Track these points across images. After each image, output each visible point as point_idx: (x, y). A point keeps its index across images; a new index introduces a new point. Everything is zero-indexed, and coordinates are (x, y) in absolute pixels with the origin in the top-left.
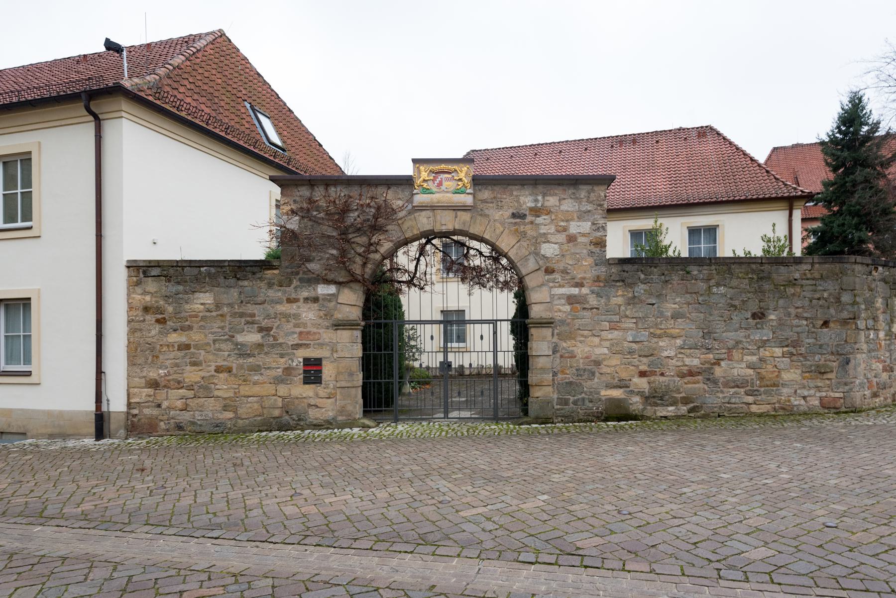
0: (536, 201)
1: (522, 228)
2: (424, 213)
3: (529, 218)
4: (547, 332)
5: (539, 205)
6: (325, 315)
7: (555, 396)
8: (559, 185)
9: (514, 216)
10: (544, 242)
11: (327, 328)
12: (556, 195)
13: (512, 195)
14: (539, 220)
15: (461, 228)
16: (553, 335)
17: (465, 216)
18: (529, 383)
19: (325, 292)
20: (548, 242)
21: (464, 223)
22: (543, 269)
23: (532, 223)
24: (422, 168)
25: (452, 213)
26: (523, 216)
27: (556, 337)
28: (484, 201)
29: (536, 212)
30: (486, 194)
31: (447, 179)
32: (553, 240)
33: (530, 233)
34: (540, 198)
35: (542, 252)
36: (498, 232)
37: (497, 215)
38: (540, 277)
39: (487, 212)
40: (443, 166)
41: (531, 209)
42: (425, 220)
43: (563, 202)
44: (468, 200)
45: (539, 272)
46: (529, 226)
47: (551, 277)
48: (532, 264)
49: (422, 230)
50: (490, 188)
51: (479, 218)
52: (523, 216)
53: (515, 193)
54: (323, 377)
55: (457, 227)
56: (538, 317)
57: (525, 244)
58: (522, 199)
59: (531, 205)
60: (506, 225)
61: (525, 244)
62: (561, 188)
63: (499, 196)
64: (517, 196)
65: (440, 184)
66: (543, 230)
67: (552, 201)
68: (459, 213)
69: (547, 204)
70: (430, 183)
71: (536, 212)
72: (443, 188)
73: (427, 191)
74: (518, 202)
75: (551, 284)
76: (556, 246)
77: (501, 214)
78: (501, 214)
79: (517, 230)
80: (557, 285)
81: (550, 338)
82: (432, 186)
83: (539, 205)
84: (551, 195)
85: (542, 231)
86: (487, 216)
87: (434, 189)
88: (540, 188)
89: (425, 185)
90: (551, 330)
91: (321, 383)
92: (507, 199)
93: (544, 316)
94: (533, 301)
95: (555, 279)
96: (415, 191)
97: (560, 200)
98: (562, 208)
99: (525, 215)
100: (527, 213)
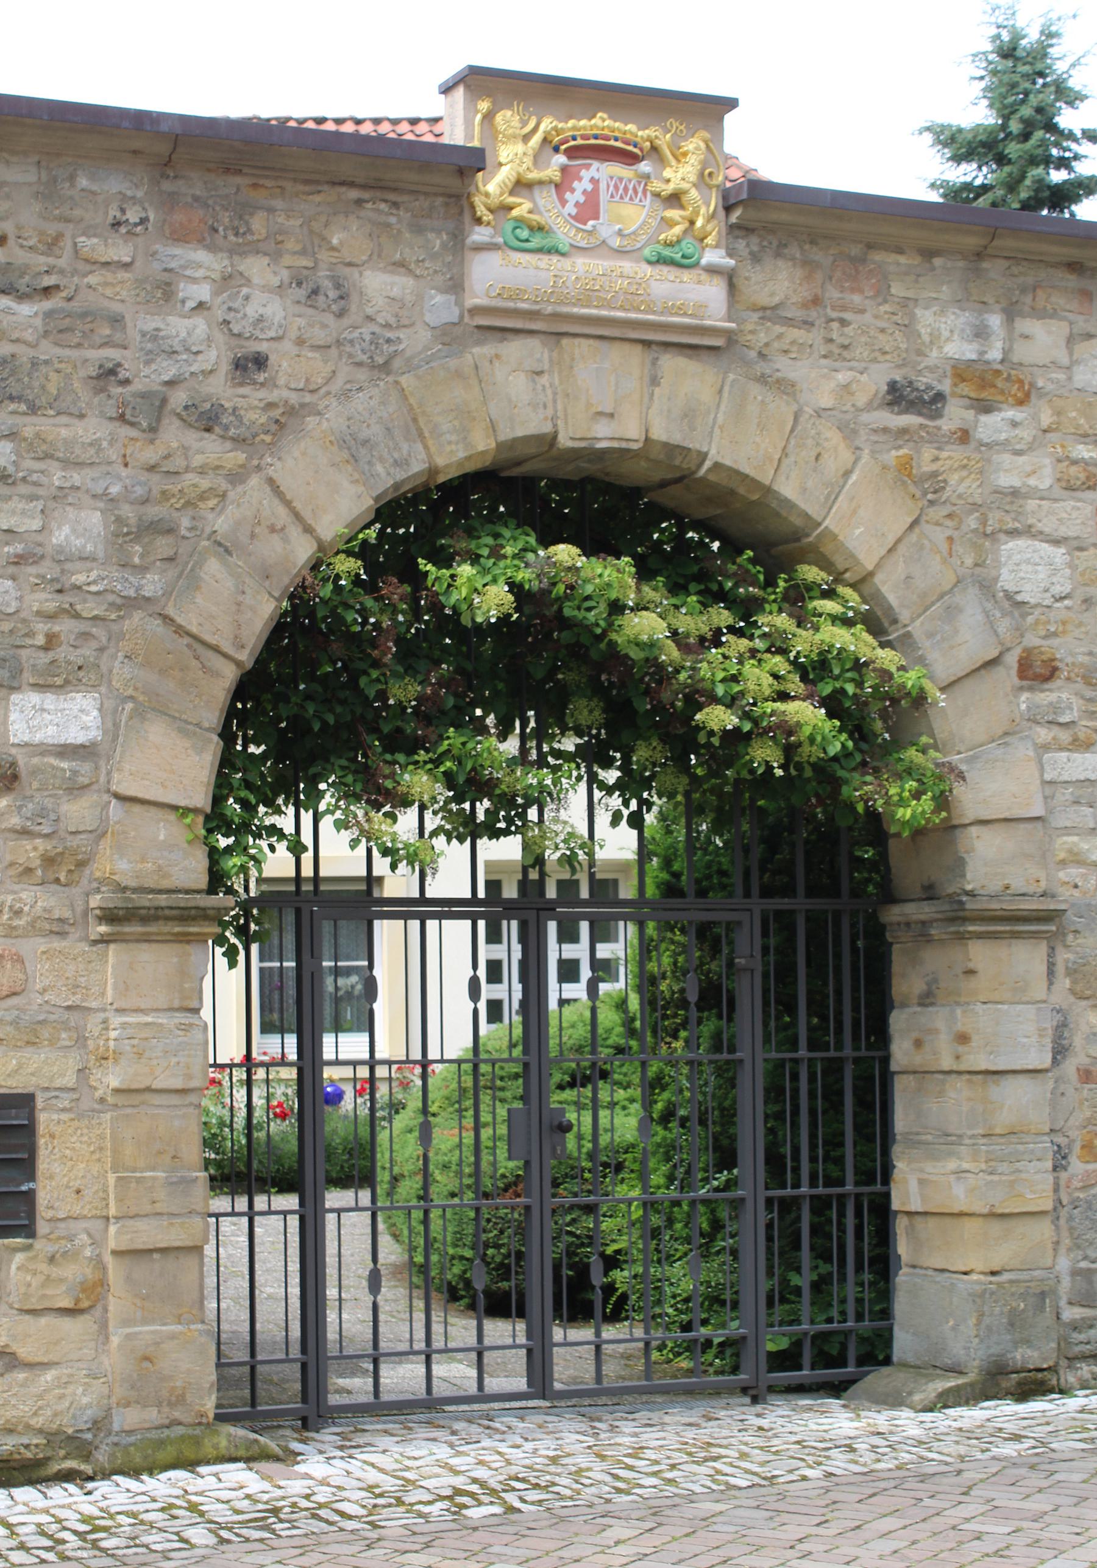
0: (981, 333)
1: (926, 459)
2: (514, 349)
3: (955, 415)
4: (1026, 959)
5: (995, 354)
6: (49, 861)
7: (1064, 1264)
8: (377, 186)
9: (898, 396)
10: (1013, 533)
11: (59, 929)
12: (1054, 315)
13: (882, 294)
14: (990, 426)
15: (676, 438)
16: (1051, 972)
17: (689, 380)
18: (895, 1205)
19: (50, 733)
20: (1028, 532)
21: (689, 415)
22: (1012, 659)
23: (964, 436)
24: (507, 119)
25: (629, 362)
26: (930, 404)
27: (1064, 983)
28: (770, 313)
29: (986, 385)
30: (778, 282)
31: (621, 191)
32: (1047, 525)
33: (962, 485)
34: (995, 321)
35: (1007, 580)
36: (832, 466)
37: (821, 383)
38: (1002, 698)
39: (784, 367)
40: (602, 122)
41: (962, 372)
42: (518, 386)
43: (1082, 349)
44: (703, 299)
45: (999, 672)
46: (953, 454)
47: (1045, 697)
48: (969, 637)
49: (506, 434)
50: (794, 250)
51: (756, 390)
52: (930, 404)
53: (897, 289)
54: (42, 1199)
55: (659, 434)
56: (994, 886)
57: (939, 535)
58: (926, 319)
59: (962, 349)
60: (863, 434)
61: (939, 535)
62: (377, 209)
63: (833, 293)
64: (905, 303)
65: (589, 209)
66: (1009, 473)
67: (1042, 340)
68: (670, 362)
69: (1023, 353)
70: (546, 199)
71: (986, 385)
72: (605, 228)
73: (535, 238)
74: (908, 328)
75: (1043, 734)
76: (1058, 554)
77: (836, 381)
78: (836, 381)
79: (905, 467)
80: (1065, 736)
81: (1039, 989)
82: (555, 213)
83: (995, 354)
84: (1040, 314)
85: (1006, 480)
86: (785, 387)
87: (564, 233)
88: (194, 185)
89: (523, 208)
90: (1043, 948)
91: (29, 1230)
92: (868, 317)
93: (1018, 884)
94: (970, 815)
95: (1056, 708)
96: (480, 235)
97: (1070, 340)
98: (1082, 377)
99: (940, 397)
100: (946, 387)
